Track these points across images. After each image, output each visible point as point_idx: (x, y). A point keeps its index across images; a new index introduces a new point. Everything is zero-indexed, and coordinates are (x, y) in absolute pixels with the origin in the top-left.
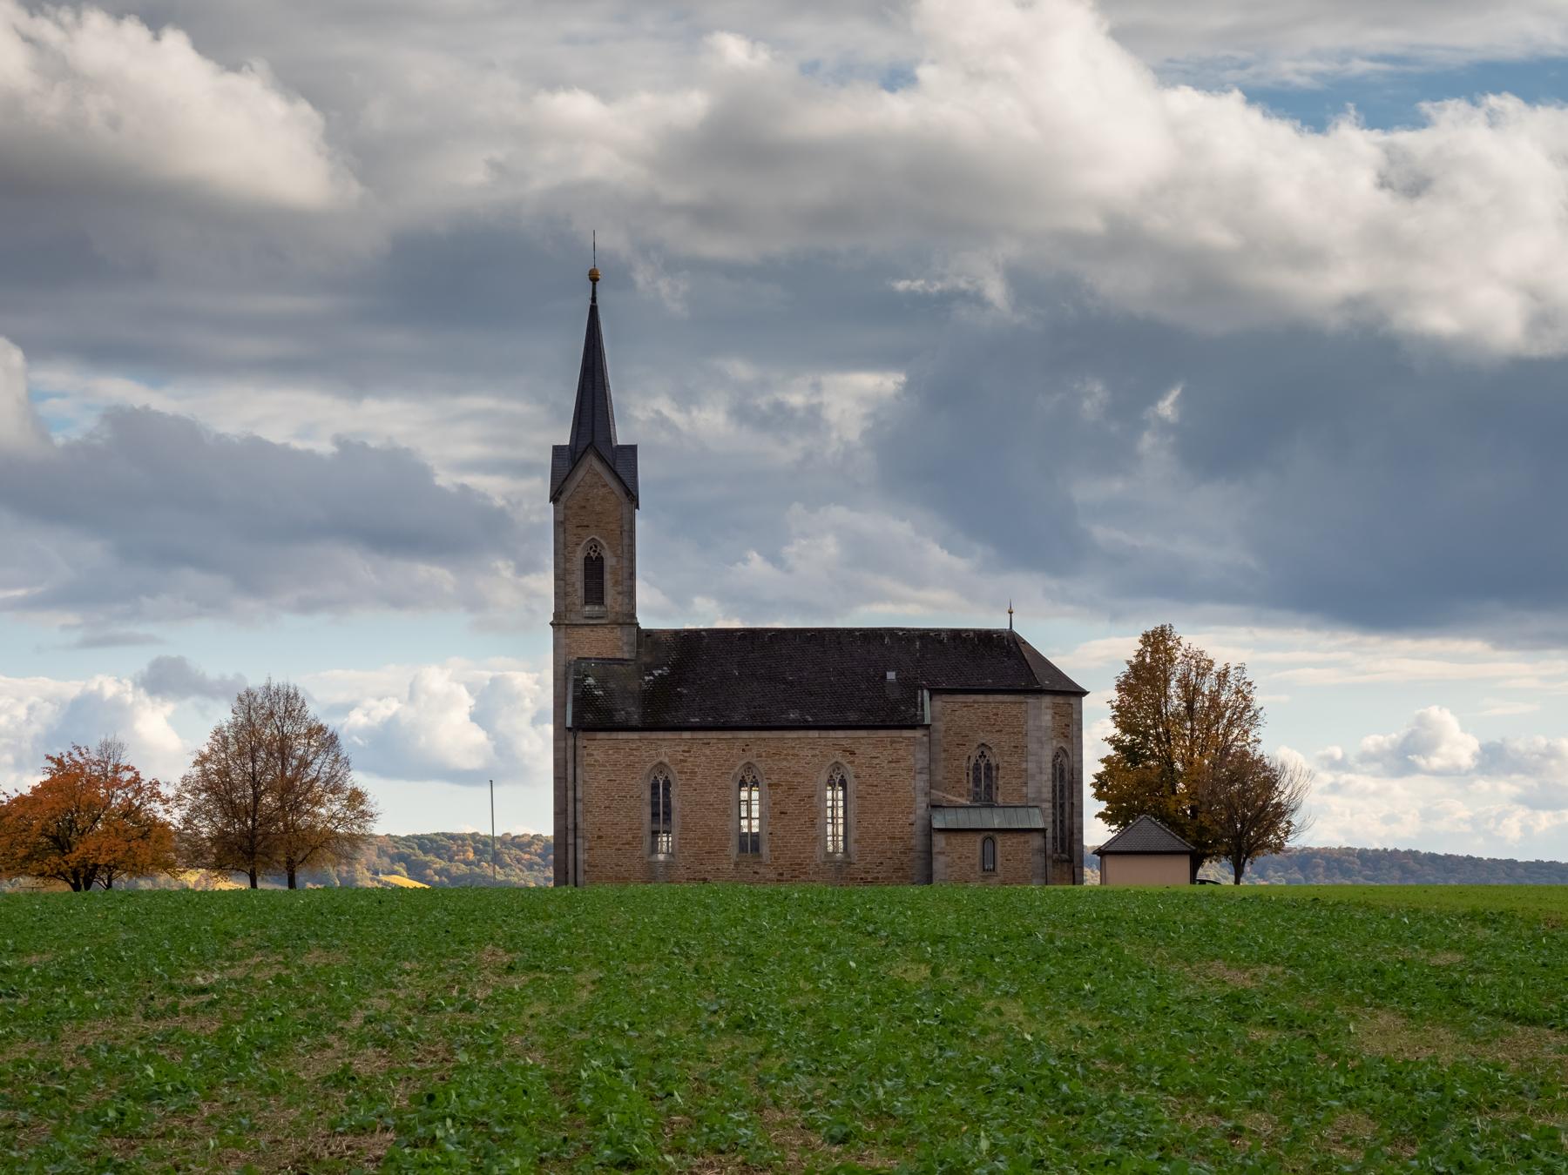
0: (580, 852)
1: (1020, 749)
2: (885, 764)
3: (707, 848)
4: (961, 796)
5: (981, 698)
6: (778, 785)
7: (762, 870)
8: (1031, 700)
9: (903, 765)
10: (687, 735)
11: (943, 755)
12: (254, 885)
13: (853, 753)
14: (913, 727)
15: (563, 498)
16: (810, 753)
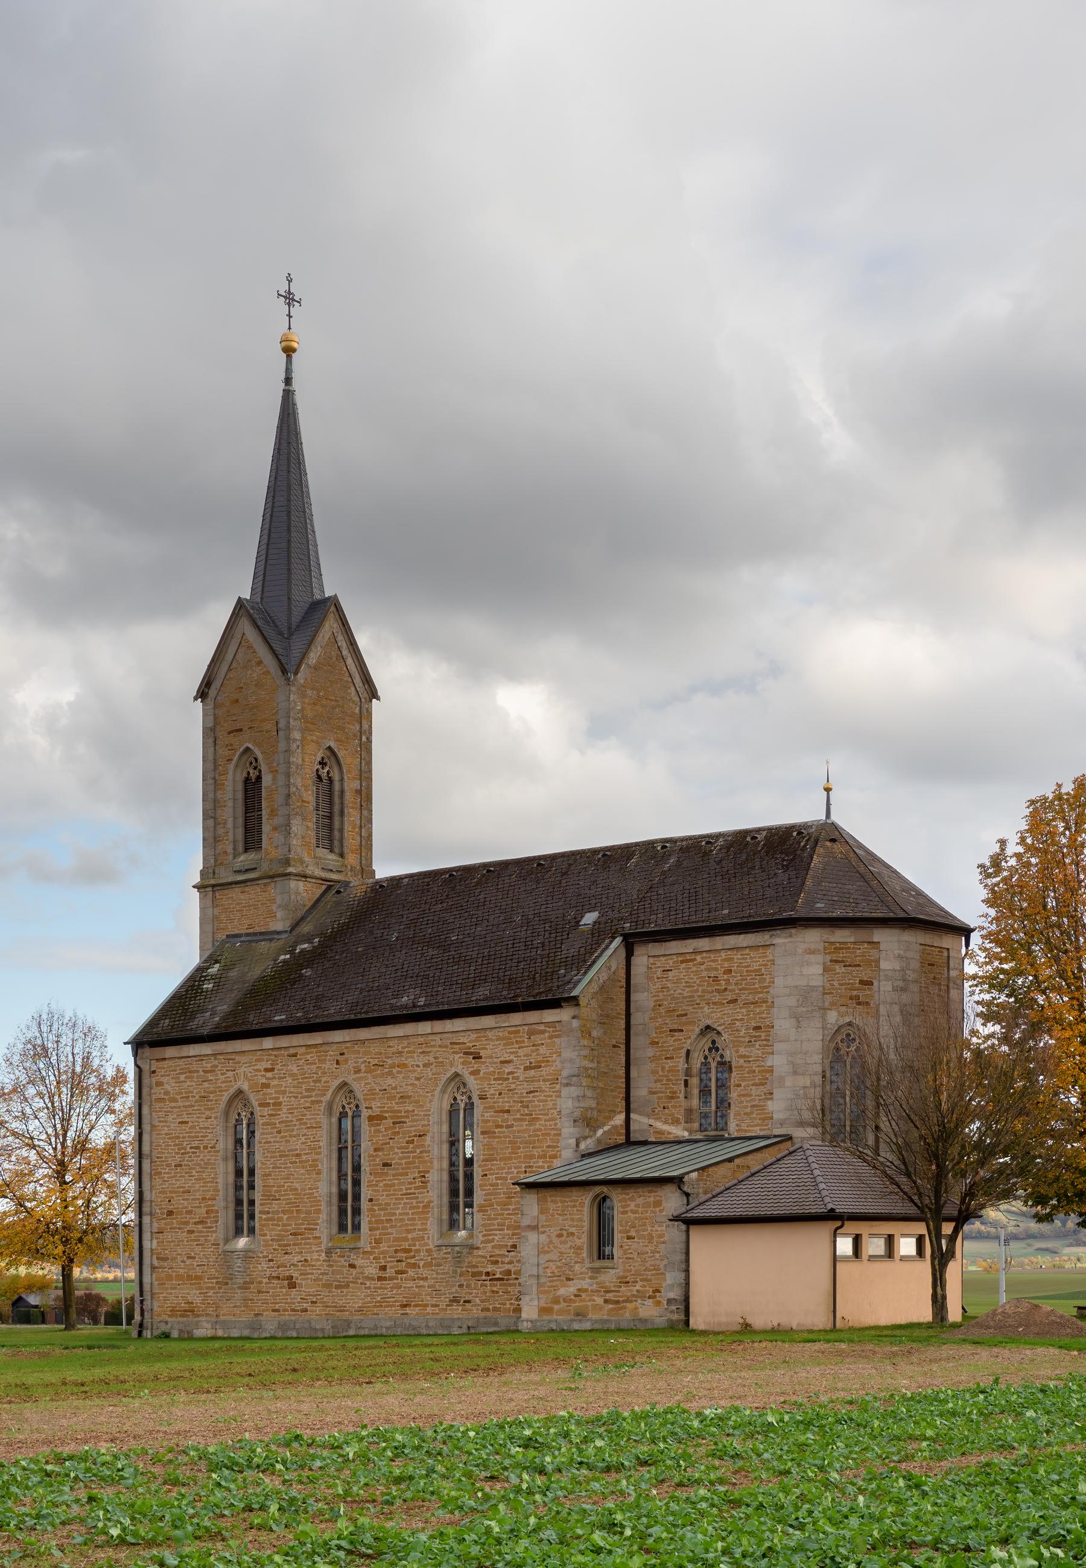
0: (147, 1236)
1: (761, 1031)
2: (520, 1073)
3: (292, 1228)
4: (676, 1122)
5: (703, 943)
6: (380, 1118)
7: (359, 1262)
8: (781, 940)
9: (545, 1071)
10: (268, 1043)
11: (650, 1052)
12: (67, 1275)
13: (477, 1057)
14: (555, 1004)
15: (212, 693)
16: (422, 1060)
